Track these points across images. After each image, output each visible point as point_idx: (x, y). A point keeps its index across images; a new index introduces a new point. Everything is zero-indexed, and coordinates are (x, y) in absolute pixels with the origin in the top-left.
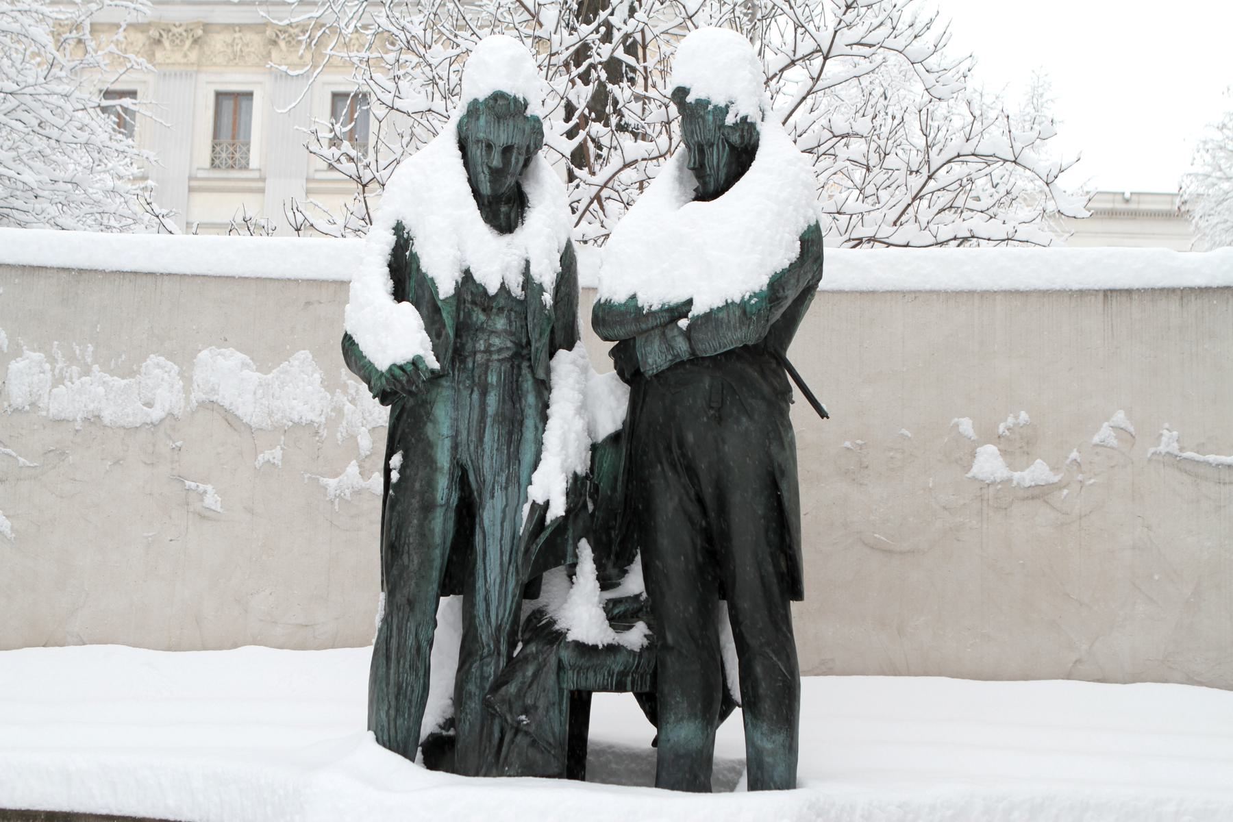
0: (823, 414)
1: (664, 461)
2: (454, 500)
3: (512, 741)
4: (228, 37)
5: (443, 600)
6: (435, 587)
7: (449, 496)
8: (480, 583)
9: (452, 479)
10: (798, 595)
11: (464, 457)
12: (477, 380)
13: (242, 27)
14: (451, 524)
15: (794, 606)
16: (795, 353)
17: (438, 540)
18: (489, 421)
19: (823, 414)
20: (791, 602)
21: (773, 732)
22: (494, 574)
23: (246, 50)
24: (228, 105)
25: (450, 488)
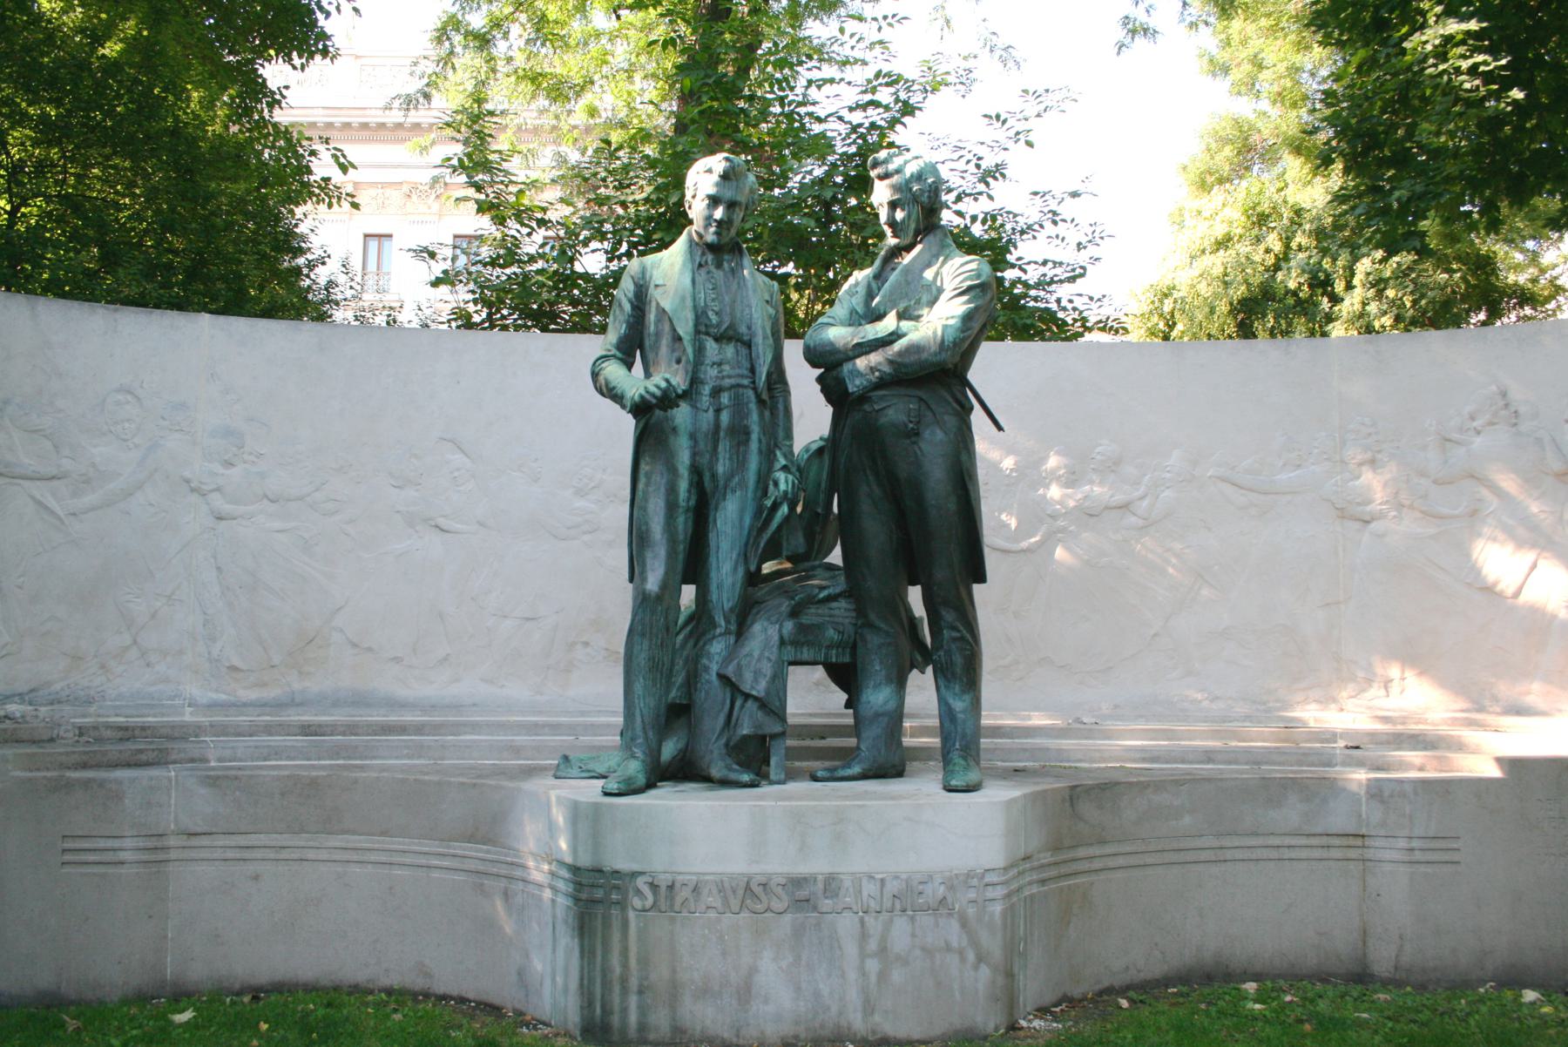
0: (1000, 428)
1: (868, 472)
2: (692, 503)
3: (742, 707)
4: (373, 192)
5: (684, 587)
6: (679, 577)
7: (689, 499)
8: (713, 574)
9: (691, 484)
10: (981, 578)
11: (704, 461)
12: (1033, 293)
13: (384, 185)
14: (690, 523)
15: (976, 588)
16: (973, 376)
17: (681, 537)
18: (722, 434)
19: (1000, 428)
20: (910, 588)
21: (963, 692)
22: (727, 567)
23: (387, 202)
24: (373, 244)
25: (689, 491)
